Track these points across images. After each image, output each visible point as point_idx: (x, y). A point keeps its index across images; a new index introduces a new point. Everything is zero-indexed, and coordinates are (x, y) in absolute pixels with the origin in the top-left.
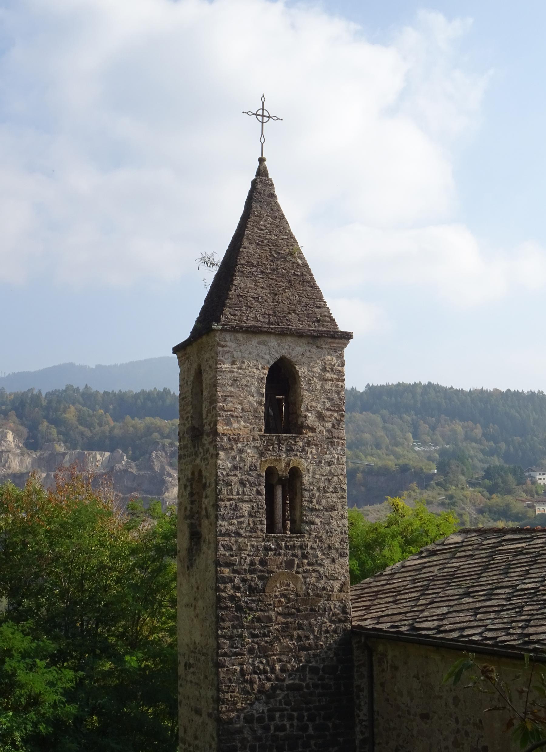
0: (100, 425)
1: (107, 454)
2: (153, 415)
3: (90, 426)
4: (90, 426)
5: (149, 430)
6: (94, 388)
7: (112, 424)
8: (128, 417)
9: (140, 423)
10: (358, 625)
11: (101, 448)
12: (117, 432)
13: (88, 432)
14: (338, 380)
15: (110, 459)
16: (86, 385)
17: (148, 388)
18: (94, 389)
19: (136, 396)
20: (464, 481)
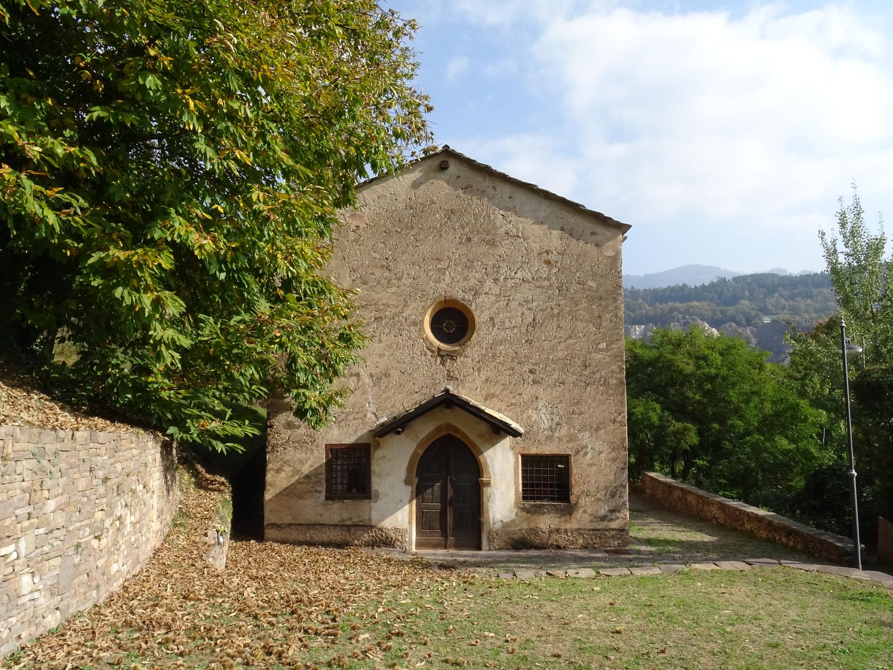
0: (640, 309)
1: (643, 327)
2: (674, 301)
3: (633, 311)
4: (633, 311)
5: (671, 310)
6: (637, 287)
7: (648, 308)
8: (658, 304)
9: (666, 307)
10: (214, 474)
11: (639, 323)
12: (651, 313)
13: (632, 315)
14: (532, 485)
15: (645, 330)
16: (630, 226)
17: (672, 284)
18: (637, 289)
19: (665, 290)
20: (111, 589)
